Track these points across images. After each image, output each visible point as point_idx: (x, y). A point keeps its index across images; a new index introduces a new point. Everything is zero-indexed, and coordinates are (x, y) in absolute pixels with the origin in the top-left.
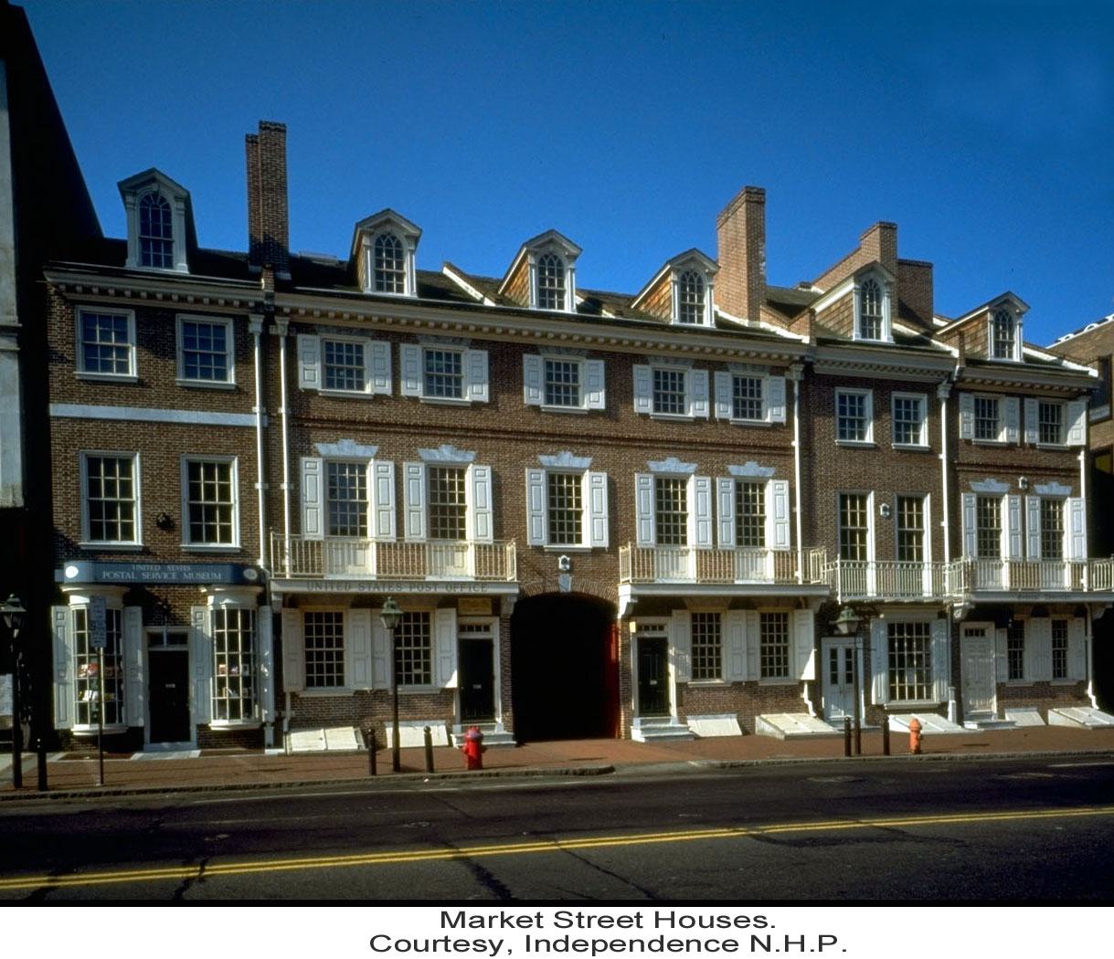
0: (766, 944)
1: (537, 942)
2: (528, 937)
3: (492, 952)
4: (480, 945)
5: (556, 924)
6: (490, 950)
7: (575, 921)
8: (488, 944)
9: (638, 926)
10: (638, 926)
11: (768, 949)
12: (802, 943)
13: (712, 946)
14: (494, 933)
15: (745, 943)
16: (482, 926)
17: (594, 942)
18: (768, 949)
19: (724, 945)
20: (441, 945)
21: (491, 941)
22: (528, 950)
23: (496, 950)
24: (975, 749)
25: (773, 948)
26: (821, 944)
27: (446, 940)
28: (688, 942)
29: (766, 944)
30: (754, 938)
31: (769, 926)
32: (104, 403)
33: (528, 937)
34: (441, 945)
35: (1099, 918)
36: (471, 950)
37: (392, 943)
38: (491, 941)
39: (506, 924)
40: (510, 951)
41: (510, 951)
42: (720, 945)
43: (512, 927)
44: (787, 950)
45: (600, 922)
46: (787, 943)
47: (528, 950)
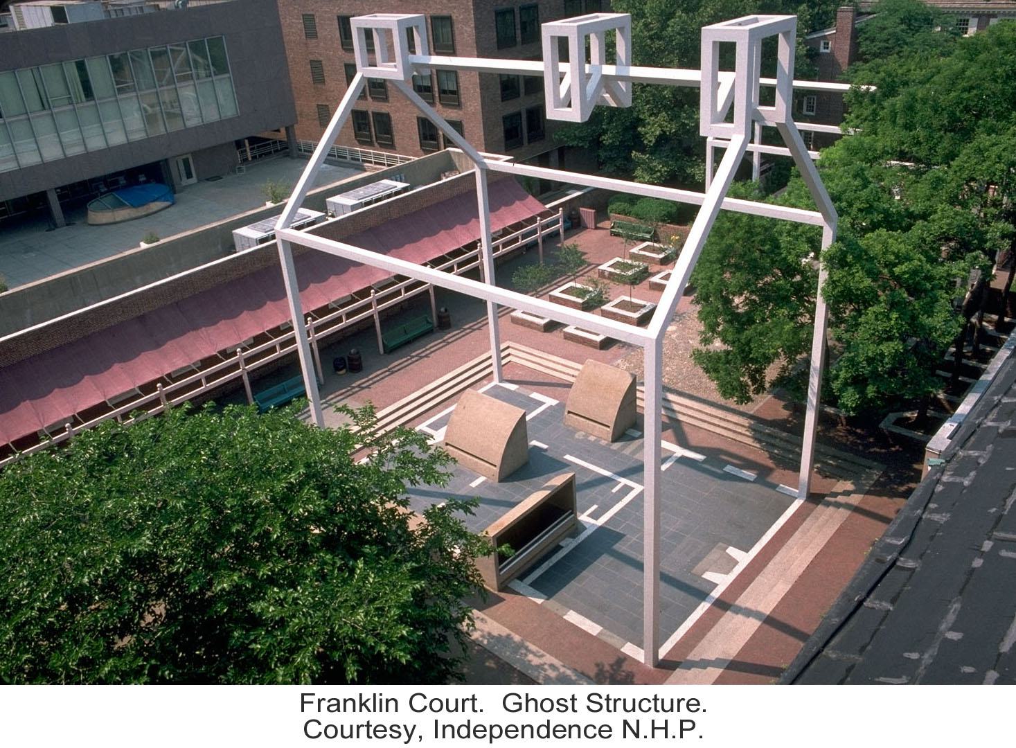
0: (410, 733)
1: (444, 727)
2: (436, 721)
3: (407, 739)
4: (395, 731)
5: (588, 707)
6: (405, 737)
7: (604, 703)
8: (402, 730)
9: (574, 711)
10: (574, 711)
11: (637, 735)
12: (666, 728)
13: (590, 732)
14: (404, 717)
15: (618, 729)
16: (338, 710)
17: (491, 727)
18: (637, 735)
19: (600, 731)
20: (363, 731)
21: (405, 726)
22: (436, 737)
23: (410, 737)
24: (740, 436)
25: (641, 735)
26: (682, 729)
27: (368, 725)
28: (570, 727)
29: (410, 733)
30: (626, 723)
31: (701, 710)
32: (382, 57)
33: (436, 721)
34: (363, 731)
35: (994, 699)
36: (388, 736)
37: (321, 728)
38: (405, 726)
39: (363, 707)
40: (420, 737)
41: (420, 737)
42: (596, 731)
43: (369, 711)
44: (681, 737)
45: (688, 705)
46: (654, 728)
47: (436, 737)
